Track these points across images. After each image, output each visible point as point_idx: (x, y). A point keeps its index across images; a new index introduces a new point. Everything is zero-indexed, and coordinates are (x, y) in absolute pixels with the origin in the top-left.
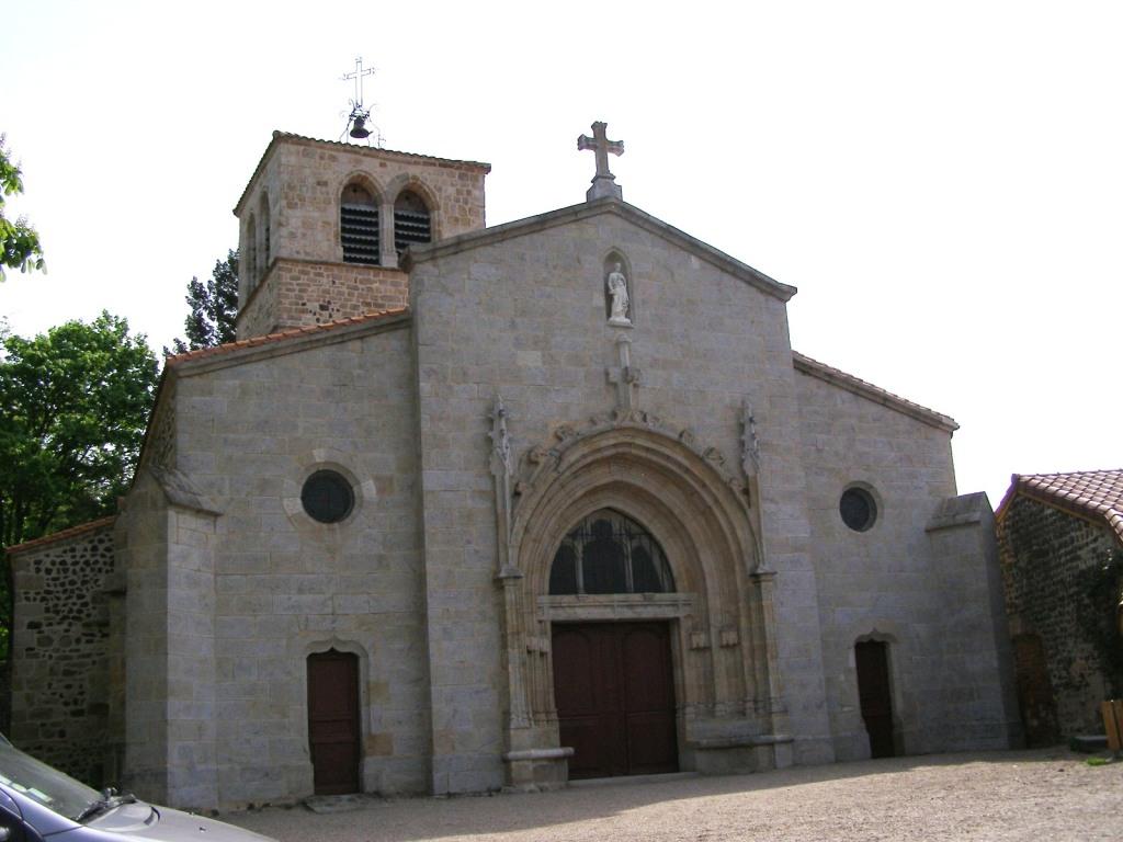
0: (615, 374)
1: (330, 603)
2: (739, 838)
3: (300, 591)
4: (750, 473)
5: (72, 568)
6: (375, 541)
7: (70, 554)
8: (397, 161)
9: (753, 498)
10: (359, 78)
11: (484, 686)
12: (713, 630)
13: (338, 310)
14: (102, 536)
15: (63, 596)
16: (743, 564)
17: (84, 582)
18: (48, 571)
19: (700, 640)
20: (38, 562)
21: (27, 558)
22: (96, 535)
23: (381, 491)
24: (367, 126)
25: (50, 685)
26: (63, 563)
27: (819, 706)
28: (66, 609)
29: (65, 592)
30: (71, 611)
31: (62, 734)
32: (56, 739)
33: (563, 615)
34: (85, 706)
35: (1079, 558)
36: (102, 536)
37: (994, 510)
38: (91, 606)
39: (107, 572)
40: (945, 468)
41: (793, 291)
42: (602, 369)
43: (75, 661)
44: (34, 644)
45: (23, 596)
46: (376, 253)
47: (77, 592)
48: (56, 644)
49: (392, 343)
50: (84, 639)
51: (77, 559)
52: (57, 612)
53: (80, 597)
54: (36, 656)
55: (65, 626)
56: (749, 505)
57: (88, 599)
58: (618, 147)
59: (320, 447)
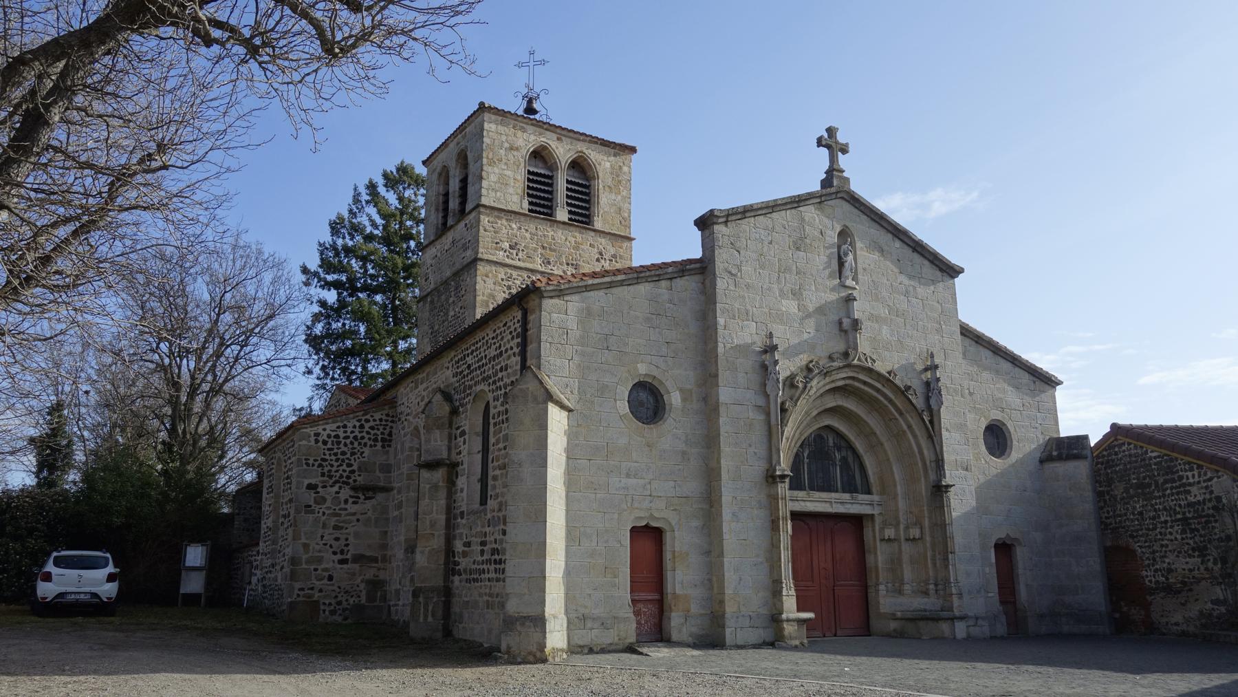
0: (846, 323)
1: (648, 486)
2: (389, 695)
3: (628, 476)
5: (343, 441)
6: (680, 439)
7: (342, 430)
8: (570, 137)
10: (531, 67)
11: (760, 560)
12: (902, 527)
13: (523, 250)
14: (368, 417)
15: (336, 464)
17: (353, 454)
18: (325, 443)
19: (889, 533)
20: (317, 435)
21: (308, 430)
22: (363, 415)
23: (684, 400)
24: (536, 105)
25: (322, 537)
26: (337, 436)
27: (979, 592)
28: (338, 474)
29: (337, 460)
30: (341, 476)
31: (330, 578)
32: (326, 581)
33: (798, 507)
34: (349, 556)
35: (1189, 492)
36: (368, 417)
37: (1092, 445)
38: (357, 473)
39: (371, 446)
40: (1052, 413)
41: (961, 271)
42: (837, 318)
43: (342, 518)
44: (312, 503)
45: (304, 462)
46: (550, 208)
47: (347, 461)
48: (328, 504)
49: (687, 285)
50: (351, 500)
51: (348, 434)
52: (330, 477)
53: (349, 465)
54: (313, 512)
55: (336, 488)
57: (355, 467)
58: (844, 150)
59: (642, 362)
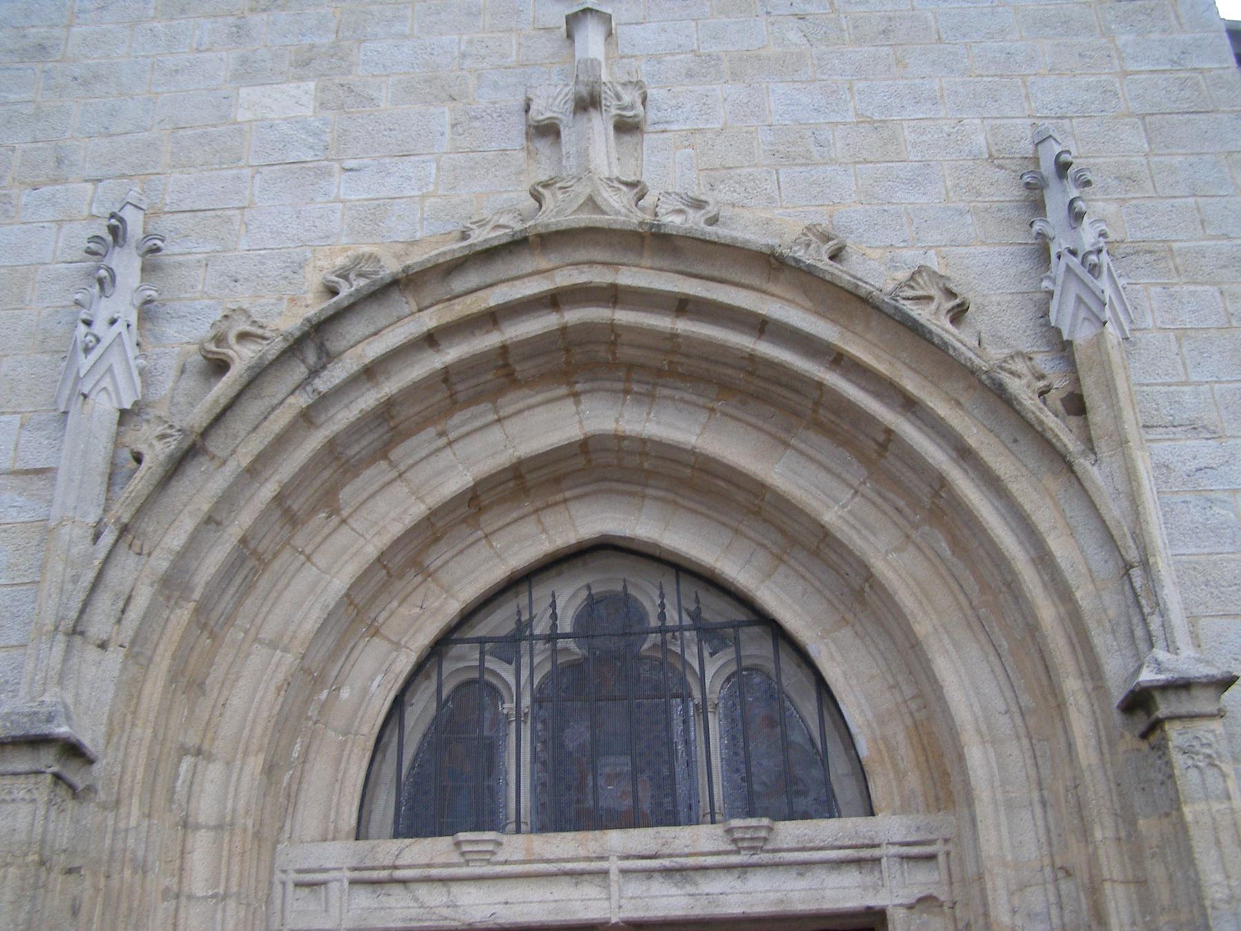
4: (1082, 335)
9: (1098, 414)
16: (1093, 670)
56: (1090, 445)
